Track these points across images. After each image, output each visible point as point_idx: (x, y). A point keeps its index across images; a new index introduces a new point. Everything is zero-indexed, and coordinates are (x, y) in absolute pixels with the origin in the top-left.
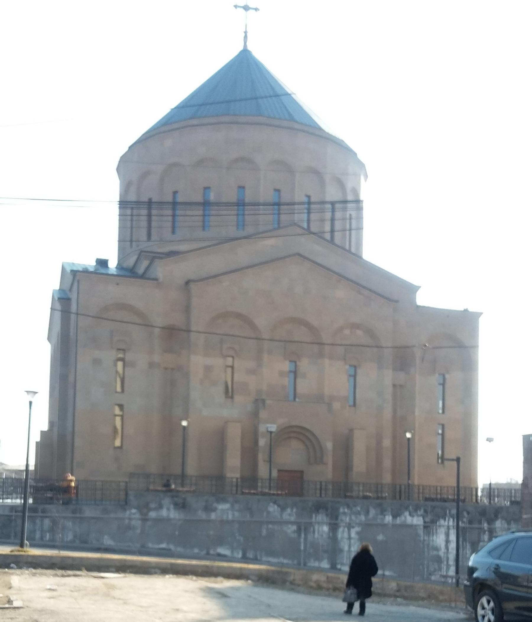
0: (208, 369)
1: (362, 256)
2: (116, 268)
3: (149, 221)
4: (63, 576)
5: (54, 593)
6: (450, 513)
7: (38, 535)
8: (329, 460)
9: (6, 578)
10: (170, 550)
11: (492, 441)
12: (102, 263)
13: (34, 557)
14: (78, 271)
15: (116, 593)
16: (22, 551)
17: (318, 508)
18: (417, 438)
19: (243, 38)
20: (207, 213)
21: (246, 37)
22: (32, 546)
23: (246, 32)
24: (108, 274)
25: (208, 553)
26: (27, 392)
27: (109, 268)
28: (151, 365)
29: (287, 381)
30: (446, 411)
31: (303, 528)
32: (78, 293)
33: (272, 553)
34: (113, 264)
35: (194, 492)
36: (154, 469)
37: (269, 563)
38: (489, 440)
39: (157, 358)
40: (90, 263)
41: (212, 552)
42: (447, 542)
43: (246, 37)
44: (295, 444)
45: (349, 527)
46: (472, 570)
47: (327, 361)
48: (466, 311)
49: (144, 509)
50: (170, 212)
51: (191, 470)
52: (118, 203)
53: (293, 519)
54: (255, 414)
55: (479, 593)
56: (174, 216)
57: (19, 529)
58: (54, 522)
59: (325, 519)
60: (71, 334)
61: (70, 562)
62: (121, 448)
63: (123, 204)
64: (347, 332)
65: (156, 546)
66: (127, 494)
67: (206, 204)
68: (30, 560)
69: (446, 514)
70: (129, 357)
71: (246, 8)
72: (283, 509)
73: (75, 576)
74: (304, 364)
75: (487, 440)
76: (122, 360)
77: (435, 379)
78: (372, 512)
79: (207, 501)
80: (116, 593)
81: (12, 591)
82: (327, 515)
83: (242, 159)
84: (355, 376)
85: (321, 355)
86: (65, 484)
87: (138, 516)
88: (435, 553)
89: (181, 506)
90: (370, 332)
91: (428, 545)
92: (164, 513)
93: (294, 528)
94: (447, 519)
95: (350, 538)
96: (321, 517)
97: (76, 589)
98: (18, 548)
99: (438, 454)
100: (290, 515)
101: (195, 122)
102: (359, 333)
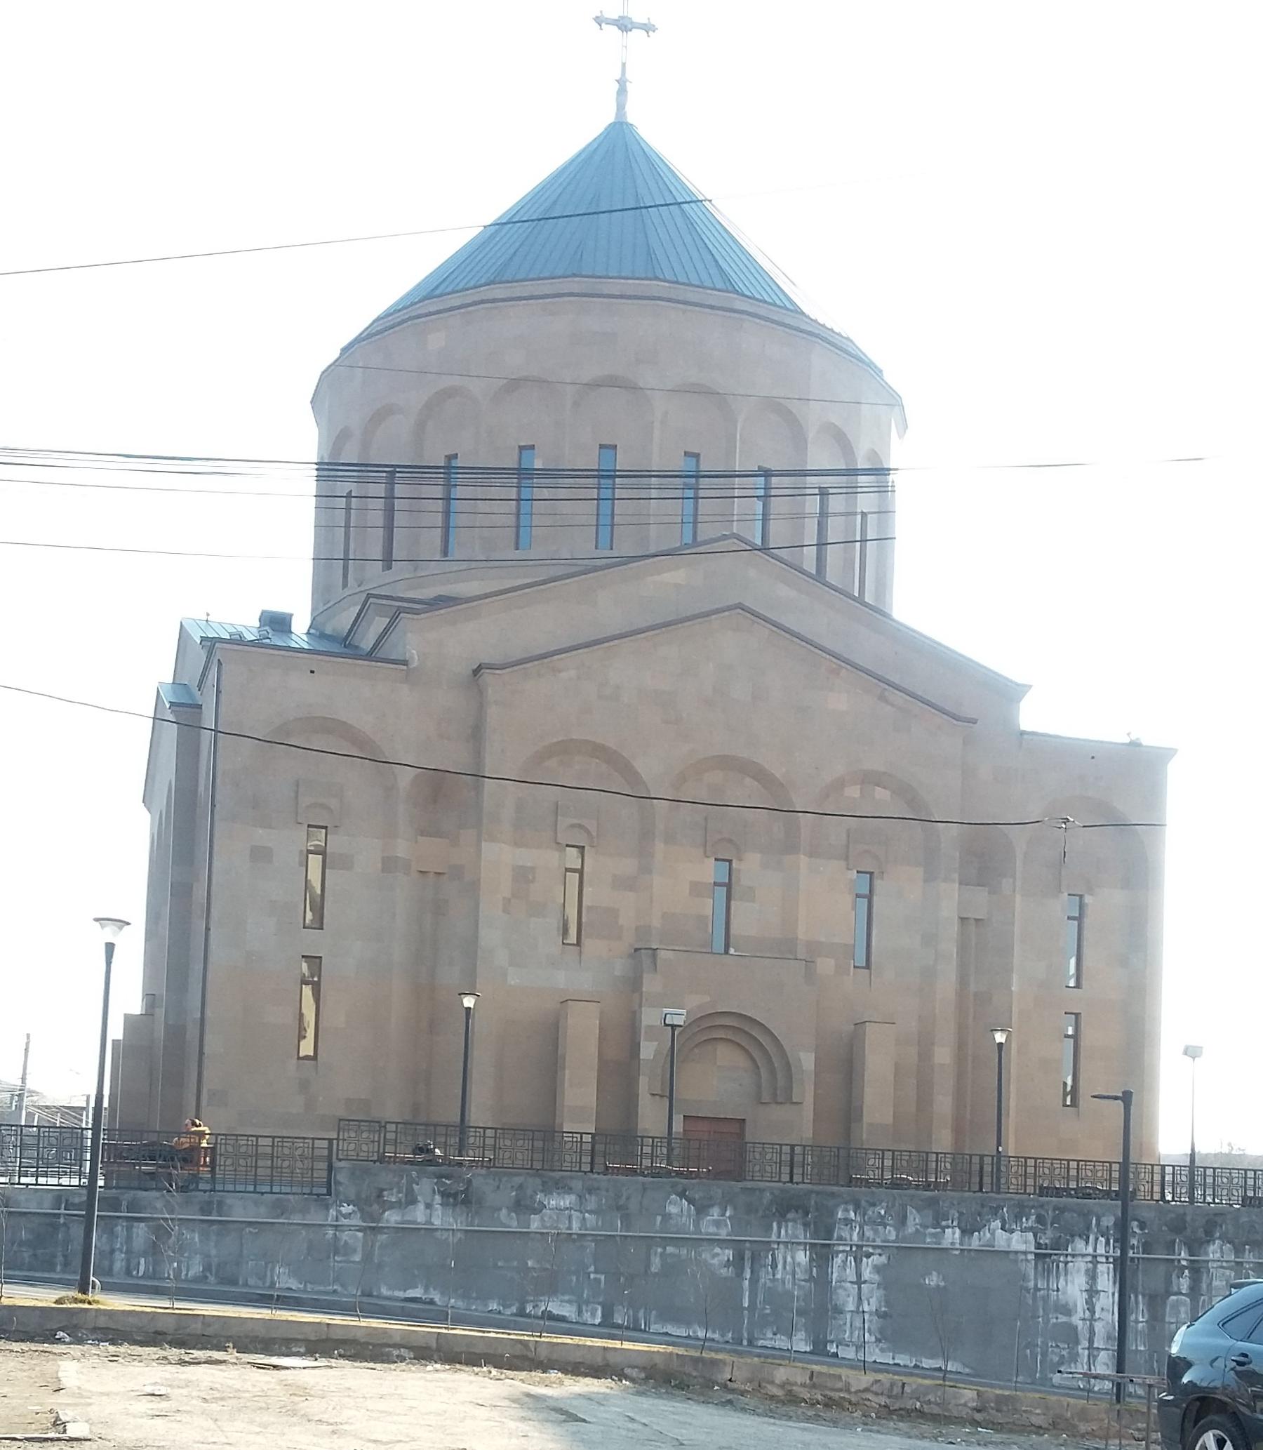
0: (523, 876)
1: (891, 609)
2: (308, 633)
3: (390, 512)
4: (182, 1362)
5: (164, 1405)
6: (1098, 1224)
7: (119, 1264)
8: (806, 1093)
9: (48, 1366)
10: (432, 1302)
11: (1199, 1056)
12: (278, 623)
13: (111, 1314)
14: (221, 640)
15: (314, 1407)
16: (83, 1301)
17: (784, 1208)
18: (1014, 1046)
19: (615, 94)
20: (526, 494)
21: (622, 91)
22: (107, 1288)
23: (624, 65)
24: (289, 649)
25: (522, 1313)
26: (97, 920)
27: (292, 633)
28: (389, 864)
29: (709, 907)
30: (1084, 983)
31: (748, 1254)
32: (218, 692)
33: (672, 1314)
34: (301, 626)
35: (491, 1165)
36: (391, 1111)
37: (666, 1338)
38: (1192, 1052)
39: (402, 848)
40: (247, 621)
41: (529, 1309)
42: (1092, 1292)
43: (622, 91)
44: (726, 1056)
45: (859, 1254)
46: (1178, 1366)
47: (803, 860)
48: (1135, 744)
49: (371, 1203)
50: (438, 491)
51: (479, 1115)
52: (316, 478)
53: (723, 1234)
54: (634, 983)
55: (1196, 1423)
56: (448, 499)
57: (77, 1245)
58: (161, 1232)
59: (802, 1235)
60: (201, 788)
61: (197, 1328)
62: (315, 1058)
63: (328, 470)
64: (853, 792)
65: (401, 1294)
66: (330, 1168)
67: (523, 474)
68: (102, 1322)
69: (1089, 1228)
70: (337, 844)
71: (624, 25)
72: (702, 1210)
73: (210, 1362)
74: (750, 867)
75: (1186, 1053)
76: (322, 852)
77: (1061, 906)
78: (914, 1219)
79: (521, 1187)
80: (314, 1407)
81: (61, 1398)
82: (806, 1225)
83: (612, 382)
84: (870, 898)
85: (790, 846)
86: (185, 1142)
87: (356, 1221)
88: (1062, 1319)
89: (461, 1199)
90: (905, 791)
91: (1046, 1299)
92: (419, 1214)
93: (729, 1254)
94: (1092, 1238)
95: (859, 1282)
96: (791, 1230)
97: (214, 1396)
98: (74, 1293)
99: (1065, 1084)
100: (717, 1224)
101: (498, 292)
102: (881, 794)
